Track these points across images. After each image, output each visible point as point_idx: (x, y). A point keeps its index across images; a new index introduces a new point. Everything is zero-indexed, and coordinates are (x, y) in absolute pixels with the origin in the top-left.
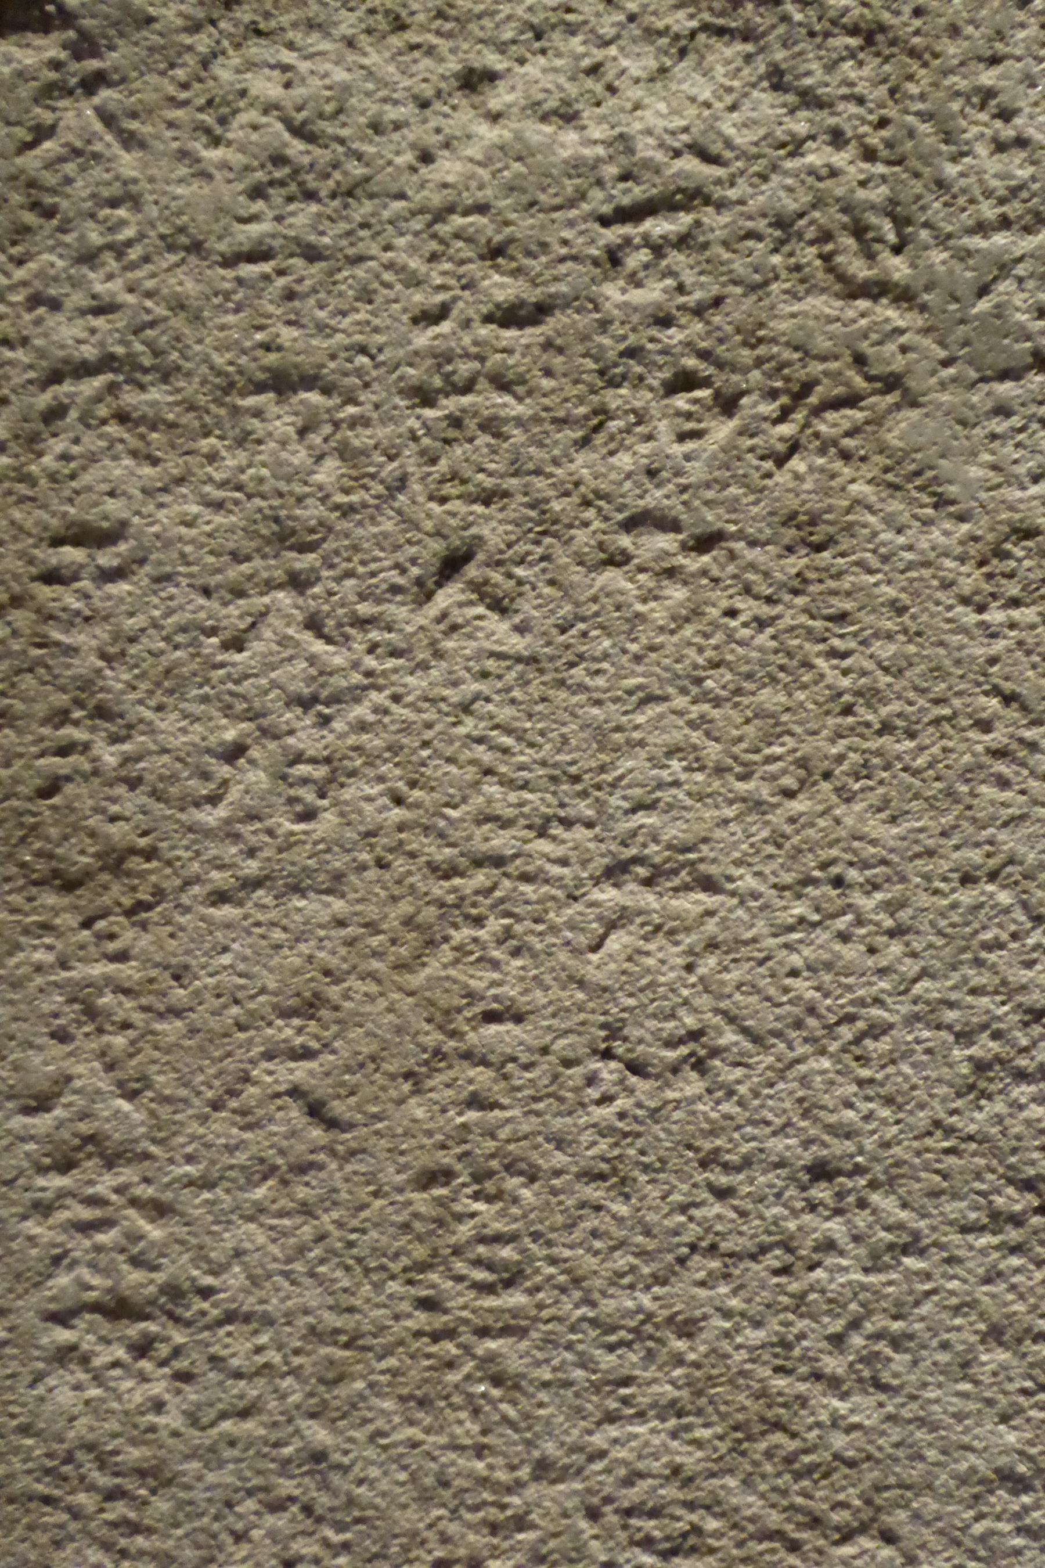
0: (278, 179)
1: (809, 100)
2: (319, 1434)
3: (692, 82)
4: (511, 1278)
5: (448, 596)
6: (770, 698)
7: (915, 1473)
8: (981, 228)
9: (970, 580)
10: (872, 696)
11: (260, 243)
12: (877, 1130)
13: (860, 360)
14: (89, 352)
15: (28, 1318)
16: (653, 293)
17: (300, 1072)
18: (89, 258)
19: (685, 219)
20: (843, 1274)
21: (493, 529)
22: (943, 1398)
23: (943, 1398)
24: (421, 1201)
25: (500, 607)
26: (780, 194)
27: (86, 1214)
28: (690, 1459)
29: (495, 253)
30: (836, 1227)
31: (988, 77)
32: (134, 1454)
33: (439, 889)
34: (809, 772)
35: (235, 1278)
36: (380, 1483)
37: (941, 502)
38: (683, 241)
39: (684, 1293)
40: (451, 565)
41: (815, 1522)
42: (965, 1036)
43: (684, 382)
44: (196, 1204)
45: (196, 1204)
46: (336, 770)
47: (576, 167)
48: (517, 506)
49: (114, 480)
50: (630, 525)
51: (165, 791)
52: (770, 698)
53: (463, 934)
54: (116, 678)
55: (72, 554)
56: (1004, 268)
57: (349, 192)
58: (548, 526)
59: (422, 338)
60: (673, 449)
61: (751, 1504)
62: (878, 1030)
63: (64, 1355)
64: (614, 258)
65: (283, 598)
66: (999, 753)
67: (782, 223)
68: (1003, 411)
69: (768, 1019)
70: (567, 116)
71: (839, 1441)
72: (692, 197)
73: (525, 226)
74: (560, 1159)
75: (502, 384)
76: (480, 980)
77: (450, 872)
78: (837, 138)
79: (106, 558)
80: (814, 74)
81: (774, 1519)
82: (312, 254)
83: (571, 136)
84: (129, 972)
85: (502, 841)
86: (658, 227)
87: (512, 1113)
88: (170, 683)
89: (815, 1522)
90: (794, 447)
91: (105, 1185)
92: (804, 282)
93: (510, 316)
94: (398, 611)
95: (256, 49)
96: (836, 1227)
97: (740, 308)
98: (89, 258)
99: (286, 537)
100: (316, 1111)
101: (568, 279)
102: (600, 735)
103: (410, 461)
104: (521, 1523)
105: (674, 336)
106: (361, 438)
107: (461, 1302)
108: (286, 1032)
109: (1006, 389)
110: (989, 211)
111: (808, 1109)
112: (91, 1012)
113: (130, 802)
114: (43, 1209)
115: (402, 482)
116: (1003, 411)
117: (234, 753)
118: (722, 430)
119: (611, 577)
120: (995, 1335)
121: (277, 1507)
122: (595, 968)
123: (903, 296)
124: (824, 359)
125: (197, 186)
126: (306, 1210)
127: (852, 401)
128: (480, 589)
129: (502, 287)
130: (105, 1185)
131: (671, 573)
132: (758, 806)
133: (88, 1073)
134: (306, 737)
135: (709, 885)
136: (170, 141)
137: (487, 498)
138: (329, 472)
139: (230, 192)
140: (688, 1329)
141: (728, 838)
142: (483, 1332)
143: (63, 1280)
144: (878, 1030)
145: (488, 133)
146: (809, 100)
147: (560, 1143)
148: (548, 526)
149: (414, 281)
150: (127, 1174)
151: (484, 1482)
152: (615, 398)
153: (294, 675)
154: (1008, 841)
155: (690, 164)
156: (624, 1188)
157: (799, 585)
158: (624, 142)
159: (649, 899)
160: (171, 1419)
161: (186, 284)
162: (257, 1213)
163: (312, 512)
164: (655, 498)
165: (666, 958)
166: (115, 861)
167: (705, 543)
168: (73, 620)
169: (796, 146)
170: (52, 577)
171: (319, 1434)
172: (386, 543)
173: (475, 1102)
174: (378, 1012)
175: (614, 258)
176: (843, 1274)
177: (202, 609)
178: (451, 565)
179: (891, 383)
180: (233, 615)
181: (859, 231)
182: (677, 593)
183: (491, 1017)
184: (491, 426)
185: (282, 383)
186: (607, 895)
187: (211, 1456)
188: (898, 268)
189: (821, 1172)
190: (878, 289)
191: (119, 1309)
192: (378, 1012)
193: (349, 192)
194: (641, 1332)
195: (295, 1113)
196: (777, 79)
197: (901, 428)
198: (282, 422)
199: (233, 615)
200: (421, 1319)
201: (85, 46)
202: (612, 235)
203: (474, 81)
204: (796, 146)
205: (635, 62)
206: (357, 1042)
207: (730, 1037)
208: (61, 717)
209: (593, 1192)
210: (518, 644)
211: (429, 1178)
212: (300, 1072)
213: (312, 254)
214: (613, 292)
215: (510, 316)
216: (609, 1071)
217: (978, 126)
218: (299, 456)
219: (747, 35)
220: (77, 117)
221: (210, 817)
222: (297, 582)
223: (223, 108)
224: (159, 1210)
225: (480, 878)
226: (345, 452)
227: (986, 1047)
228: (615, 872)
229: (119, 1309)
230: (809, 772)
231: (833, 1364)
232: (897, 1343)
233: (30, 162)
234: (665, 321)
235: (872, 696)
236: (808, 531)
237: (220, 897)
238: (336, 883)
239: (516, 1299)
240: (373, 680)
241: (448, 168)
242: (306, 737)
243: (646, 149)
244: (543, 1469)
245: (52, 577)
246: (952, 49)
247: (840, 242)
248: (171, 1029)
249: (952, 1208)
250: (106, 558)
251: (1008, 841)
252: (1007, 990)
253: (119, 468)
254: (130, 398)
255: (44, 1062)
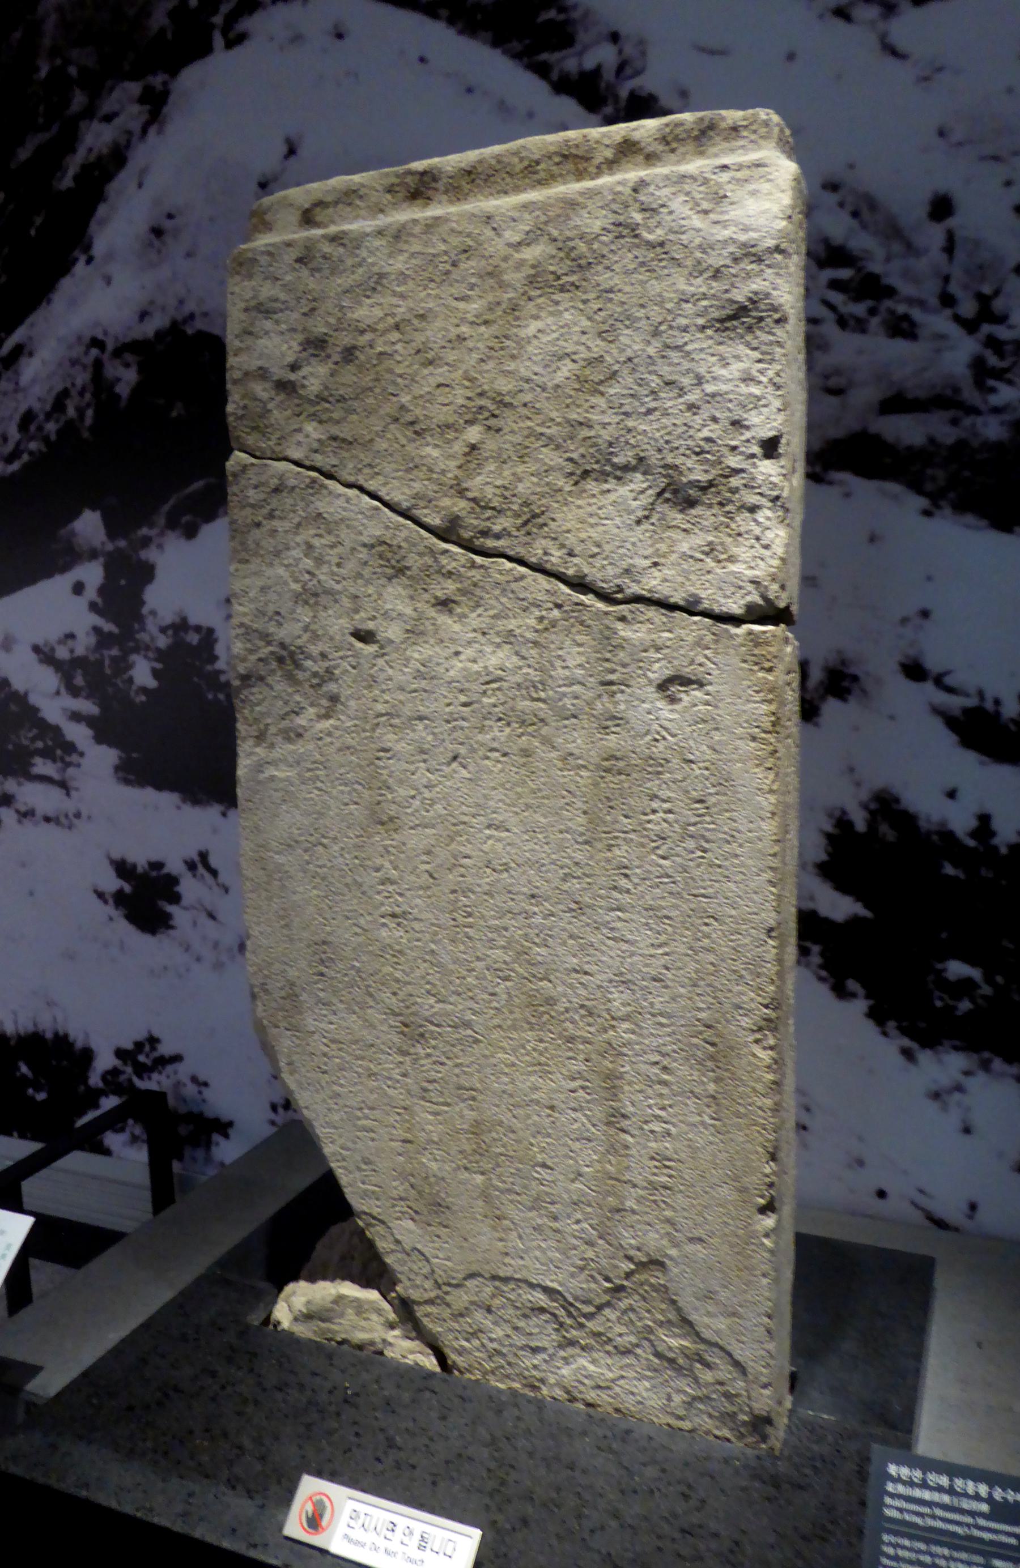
0: (419, 675)
1: (524, 658)
2: (433, 946)
3: (500, 654)
4: (470, 915)
5: (455, 765)
6: (519, 790)
7: (554, 967)
8: (560, 686)
9: (560, 764)
10: (540, 790)
12: (544, 888)
13: (535, 716)
15: (376, 916)
16: (492, 700)
17: (427, 867)
18: (383, 691)
20: (538, 920)
21: (463, 750)
22: (561, 951)
23: (561, 951)
24: (452, 896)
25: (465, 767)
26: (518, 679)
28: (508, 959)
29: (461, 691)
30: (536, 909)
31: (560, 653)
32: (397, 947)
33: (454, 828)
34: (528, 807)
35: (416, 911)
36: (445, 959)
37: (553, 747)
38: (499, 689)
39: (506, 921)
40: (455, 758)
41: (534, 976)
42: (562, 868)
43: (500, 719)
44: (408, 894)
46: (433, 802)
47: (478, 673)
48: (467, 746)
49: (389, 739)
51: (489, 529)
52: (519, 790)
53: (459, 839)
54: (391, 781)
55: (382, 754)
56: (564, 695)
57: (432, 678)
58: (473, 750)
59: (448, 709)
60: (498, 734)
61: (521, 971)
62: (543, 865)
63: (384, 925)
64: (485, 692)
65: (422, 764)
67: (519, 685)
68: (566, 727)
69: (520, 861)
70: (475, 661)
71: (539, 958)
72: (500, 679)
73: (467, 685)
75: (463, 719)
76: (462, 849)
77: (454, 825)
78: (529, 666)
79: (388, 755)
80: (524, 652)
81: (526, 975)
82: (425, 691)
85: (465, 819)
86: (495, 685)
87: (469, 879)
88: (401, 782)
89: (534, 976)
90: (522, 734)
92: (524, 698)
93: (465, 705)
94: (444, 768)
95: (415, 647)
96: (536, 909)
97: (511, 703)
98: (383, 691)
99: (423, 752)
100: (431, 876)
101: (475, 697)
102: (485, 796)
103: (446, 736)
104: (473, 970)
105: (497, 710)
106: (436, 731)
107: (460, 919)
108: (424, 858)
109: (566, 722)
110: (561, 682)
111: (530, 882)
112: (388, 852)
113: (394, 807)
114: (379, 893)
115: (444, 740)
116: (566, 727)
117: (413, 797)
118: (508, 730)
119: (487, 762)
120: (571, 937)
121: (425, 961)
122: (486, 847)
123: (544, 701)
124: (664, 801)
125: (402, 675)
126: (429, 897)
127: (533, 724)
128: (461, 763)
129: (463, 699)
130: (391, 888)
131: (499, 761)
132: (517, 813)
133: (387, 865)
134: (427, 795)
135: (508, 830)
136: (398, 667)
137: (462, 744)
138: (430, 738)
139: (410, 678)
140: (506, 929)
141: (512, 821)
143: (383, 909)
144: (543, 865)
145: (460, 665)
146: (524, 658)
147: (479, 886)
148: (473, 750)
149: (445, 697)
150: (395, 887)
152: (487, 723)
153: (424, 781)
154: (570, 824)
155: (500, 672)
156: (492, 897)
157: (524, 765)
158: (486, 667)
159: (495, 833)
160: (404, 941)
161: (401, 697)
162: (420, 897)
163: (427, 746)
164: (495, 745)
165: (499, 846)
166: (391, 819)
167: (505, 755)
168: (384, 768)
169: (520, 668)
170: (378, 759)
171: (433, 946)
172: (442, 753)
173: (463, 876)
174: (442, 854)
175: (485, 692)
176: (538, 920)
177: (406, 766)
178: (455, 758)
179: (542, 720)
180: (412, 768)
181: (534, 687)
182: (500, 766)
184: (462, 728)
185: (421, 718)
186: (487, 832)
187: (411, 949)
188: (542, 695)
189: (533, 896)
190: (539, 700)
191: (394, 916)
192: (442, 854)
193: (432, 678)
194: (496, 929)
195: (426, 876)
196: (517, 654)
197: (545, 730)
198: (421, 727)
199: (412, 768)
200: (453, 923)
201: (382, 647)
202: (484, 687)
203: (457, 653)
204: (520, 668)
205: (489, 649)
206: (438, 861)
207: (513, 865)
208: (380, 788)
209: (486, 897)
210: (468, 776)
211: (454, 892)
212: (427, 867)
213: (425, 691)
214: (485, 700)
215: (465, 705)
216: (488, 871)
217: (558, 663)
218: (424, 734)
219: (511, 643)
220: (381, 662)
221: (409, 811)
222: (425, 761)
223: (408, 660)
224: (401, 895)
225: (462, 827)
226: (434, 734)
227: (567, 871)
228: (489, 827)
229: (394, 916)
230: (528, 807)
231: (537, 940)
232: (550, 936)
233: (372, 672)
234: (495, 706)
235: (540, 790)
236: (526, 753)
237: (412, 828)
238: (433, 827)
239: (471, 920)
240: (440, 782)
241: (452, 673)
242: (427, 795)
243: (491, 669)
244: (478, 959)
245: (378, 759)
246: (552, 646)
247: (530, 688)
248: (402, 856)
249: (561, 907)
250: (388, 755)
251: (570, 824)
252: (570, 858)
253: (391, 736)
254: (393, 721)
255: (379, 861)
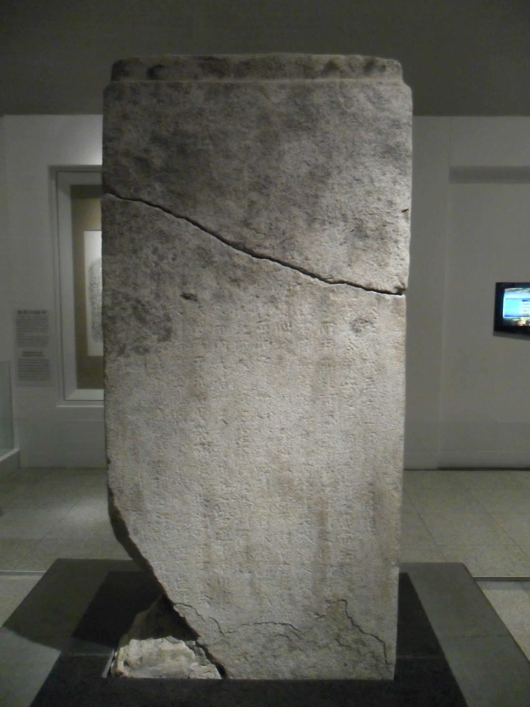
11: (206, 645)
14: (199, 337)
19: (266, 323)
21: (244, 357)
27: (198, 433)
32: (204, 461)
45: (211, 432)
50: (260, 356)
66: (302, 382)
74: (252, 427)
76: (244, 407)
83: (253, 314)
84: (203, 406)
91: (201, 430)
100: (225, 422)
111: (281, 422)
142: (244, 447)
151: (244, 464)
155: (267, 317)
183: (245, 411)
210: (247, 369)
227: (301, 415)
